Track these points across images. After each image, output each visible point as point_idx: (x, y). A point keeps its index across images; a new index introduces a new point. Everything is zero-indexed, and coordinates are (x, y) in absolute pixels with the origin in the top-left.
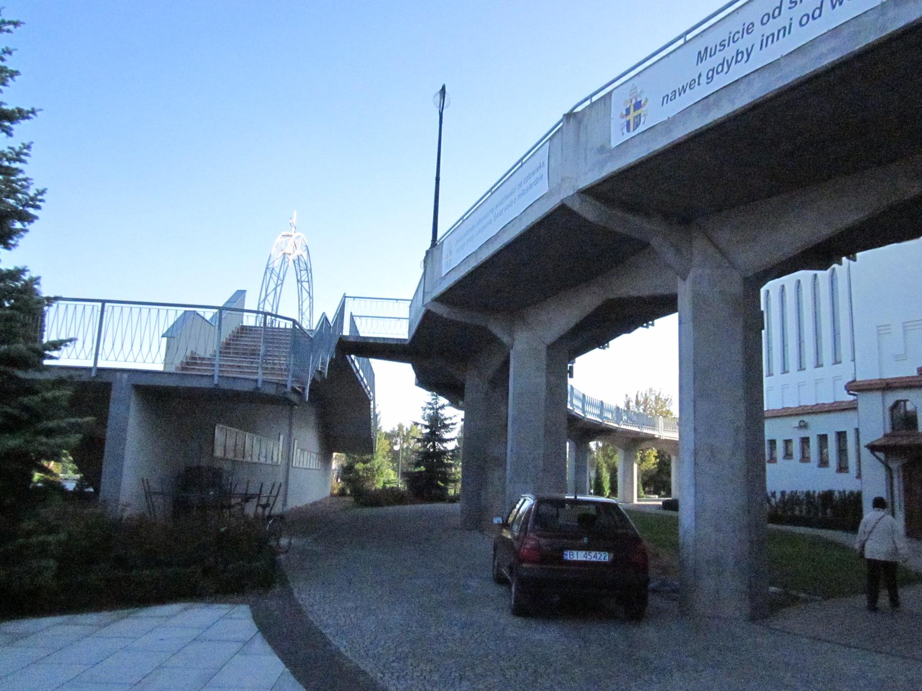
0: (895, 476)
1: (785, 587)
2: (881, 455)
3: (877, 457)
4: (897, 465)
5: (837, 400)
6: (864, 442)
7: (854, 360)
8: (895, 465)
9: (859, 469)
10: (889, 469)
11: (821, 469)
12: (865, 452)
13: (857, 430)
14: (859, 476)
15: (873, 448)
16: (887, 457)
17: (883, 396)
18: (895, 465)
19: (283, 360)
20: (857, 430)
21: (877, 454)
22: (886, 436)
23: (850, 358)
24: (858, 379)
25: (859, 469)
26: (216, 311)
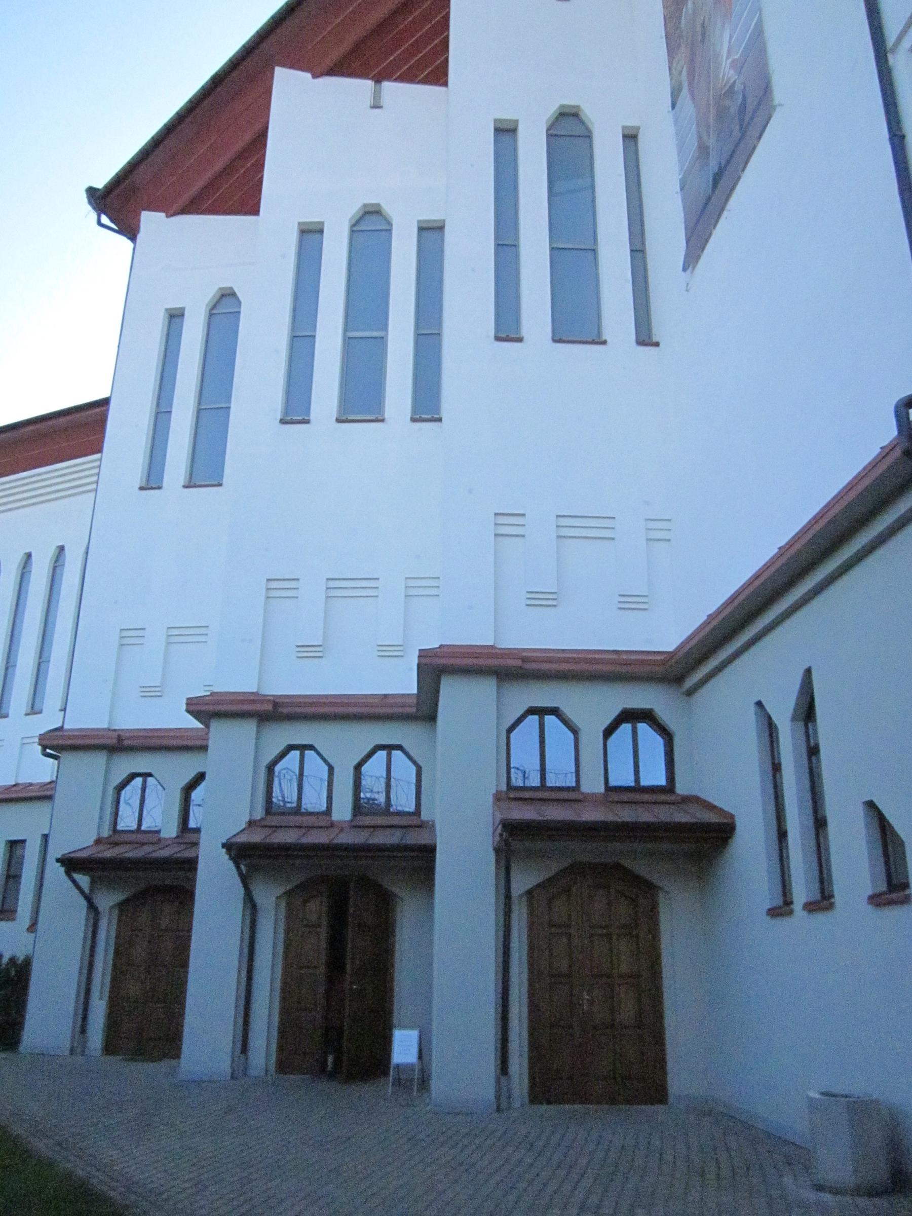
0: (103, 924)
1: (570, 1078)
3: (74, 882)
4: (118, 897)
5: (21, 781)
6: (57, 850)
7: (64, 710)
8: (107, 901)
9: (36, 912)
10: (92, 907)
11: (84, 196)
13: (46, 837)
14: (33, 928)
15: (71, 864)
16: (93, 882)
17: (109, 760)
18: (107, 901)
20: (46, 837)
21: (77, 876)
22: (98, 841)
23: (59, 705)
24: (66, 727)
25: (36, 912)
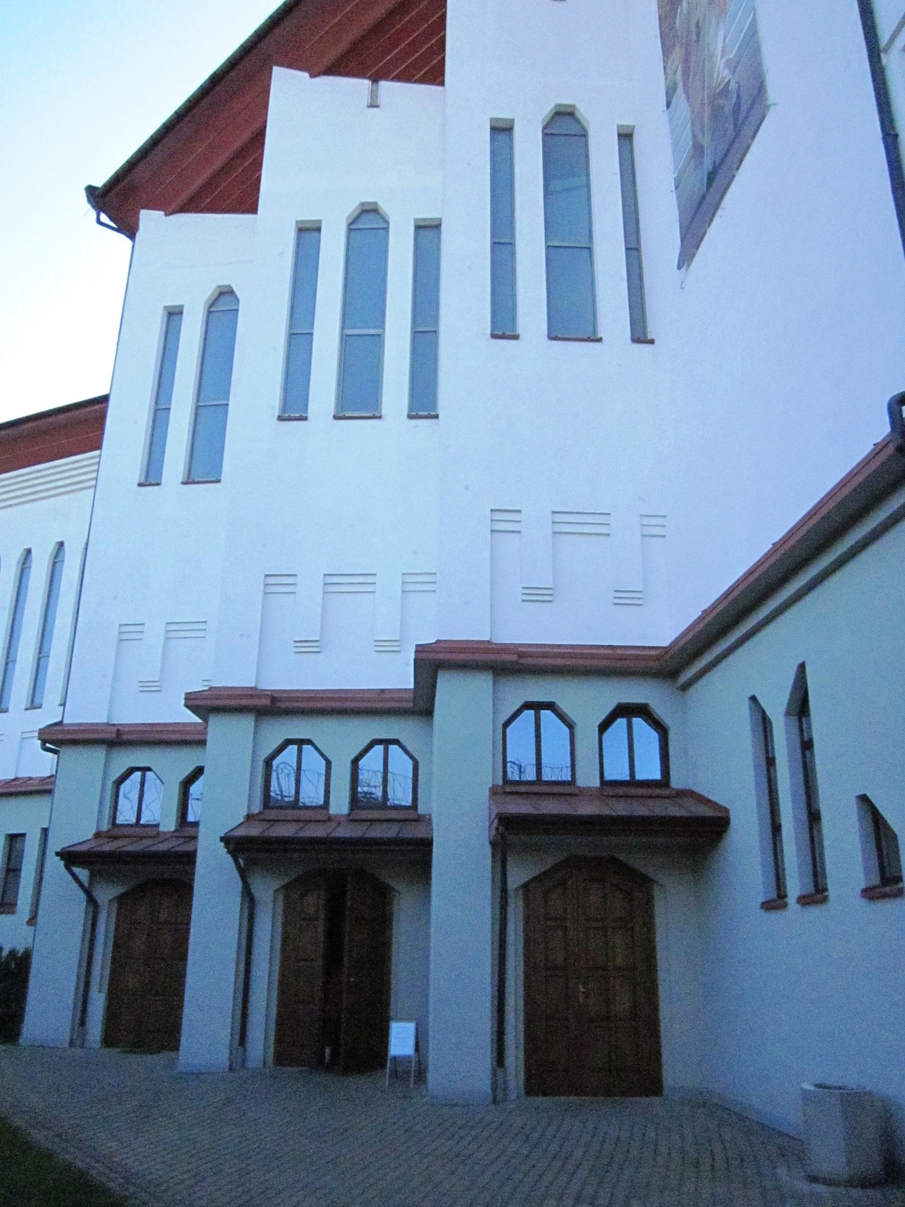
0: (103, 917)
2: (83, 874)
3: (74, 875)
5: (21, 775)
6: (56, 844)
7: (63, 704)
8: (106, 894)
10: (91, 900)
12: (55, 865)
13: (45, 831)
14: (32, 921)
15: (70, 858)
16: (92, 876)
17: (495, 683)
18: (106, 894)
19: (557, 771)
20: (45, 831)
23: (58, 700)
24: (66, 721)
26: (379, 792)
